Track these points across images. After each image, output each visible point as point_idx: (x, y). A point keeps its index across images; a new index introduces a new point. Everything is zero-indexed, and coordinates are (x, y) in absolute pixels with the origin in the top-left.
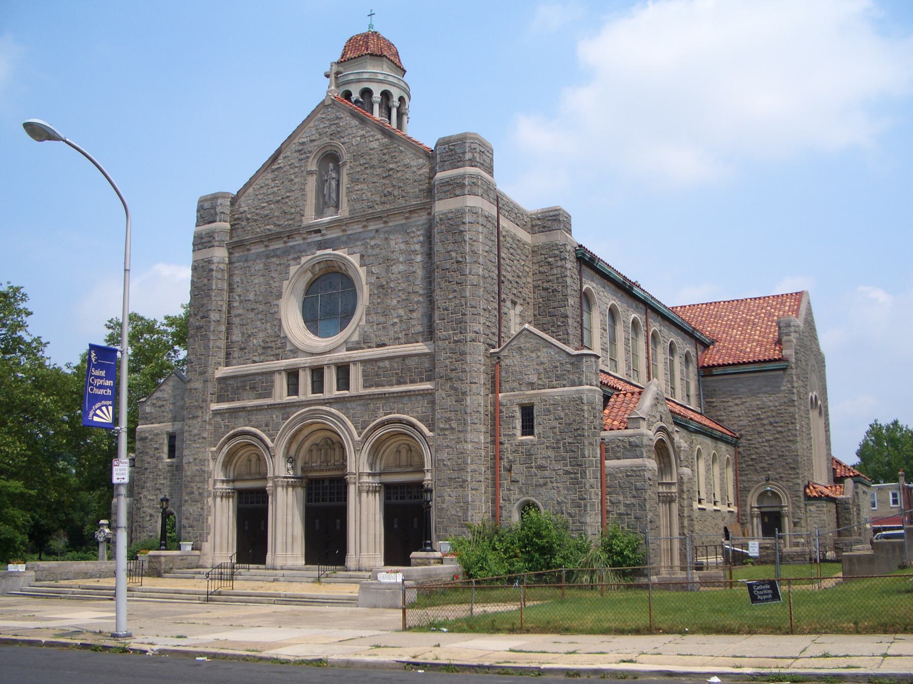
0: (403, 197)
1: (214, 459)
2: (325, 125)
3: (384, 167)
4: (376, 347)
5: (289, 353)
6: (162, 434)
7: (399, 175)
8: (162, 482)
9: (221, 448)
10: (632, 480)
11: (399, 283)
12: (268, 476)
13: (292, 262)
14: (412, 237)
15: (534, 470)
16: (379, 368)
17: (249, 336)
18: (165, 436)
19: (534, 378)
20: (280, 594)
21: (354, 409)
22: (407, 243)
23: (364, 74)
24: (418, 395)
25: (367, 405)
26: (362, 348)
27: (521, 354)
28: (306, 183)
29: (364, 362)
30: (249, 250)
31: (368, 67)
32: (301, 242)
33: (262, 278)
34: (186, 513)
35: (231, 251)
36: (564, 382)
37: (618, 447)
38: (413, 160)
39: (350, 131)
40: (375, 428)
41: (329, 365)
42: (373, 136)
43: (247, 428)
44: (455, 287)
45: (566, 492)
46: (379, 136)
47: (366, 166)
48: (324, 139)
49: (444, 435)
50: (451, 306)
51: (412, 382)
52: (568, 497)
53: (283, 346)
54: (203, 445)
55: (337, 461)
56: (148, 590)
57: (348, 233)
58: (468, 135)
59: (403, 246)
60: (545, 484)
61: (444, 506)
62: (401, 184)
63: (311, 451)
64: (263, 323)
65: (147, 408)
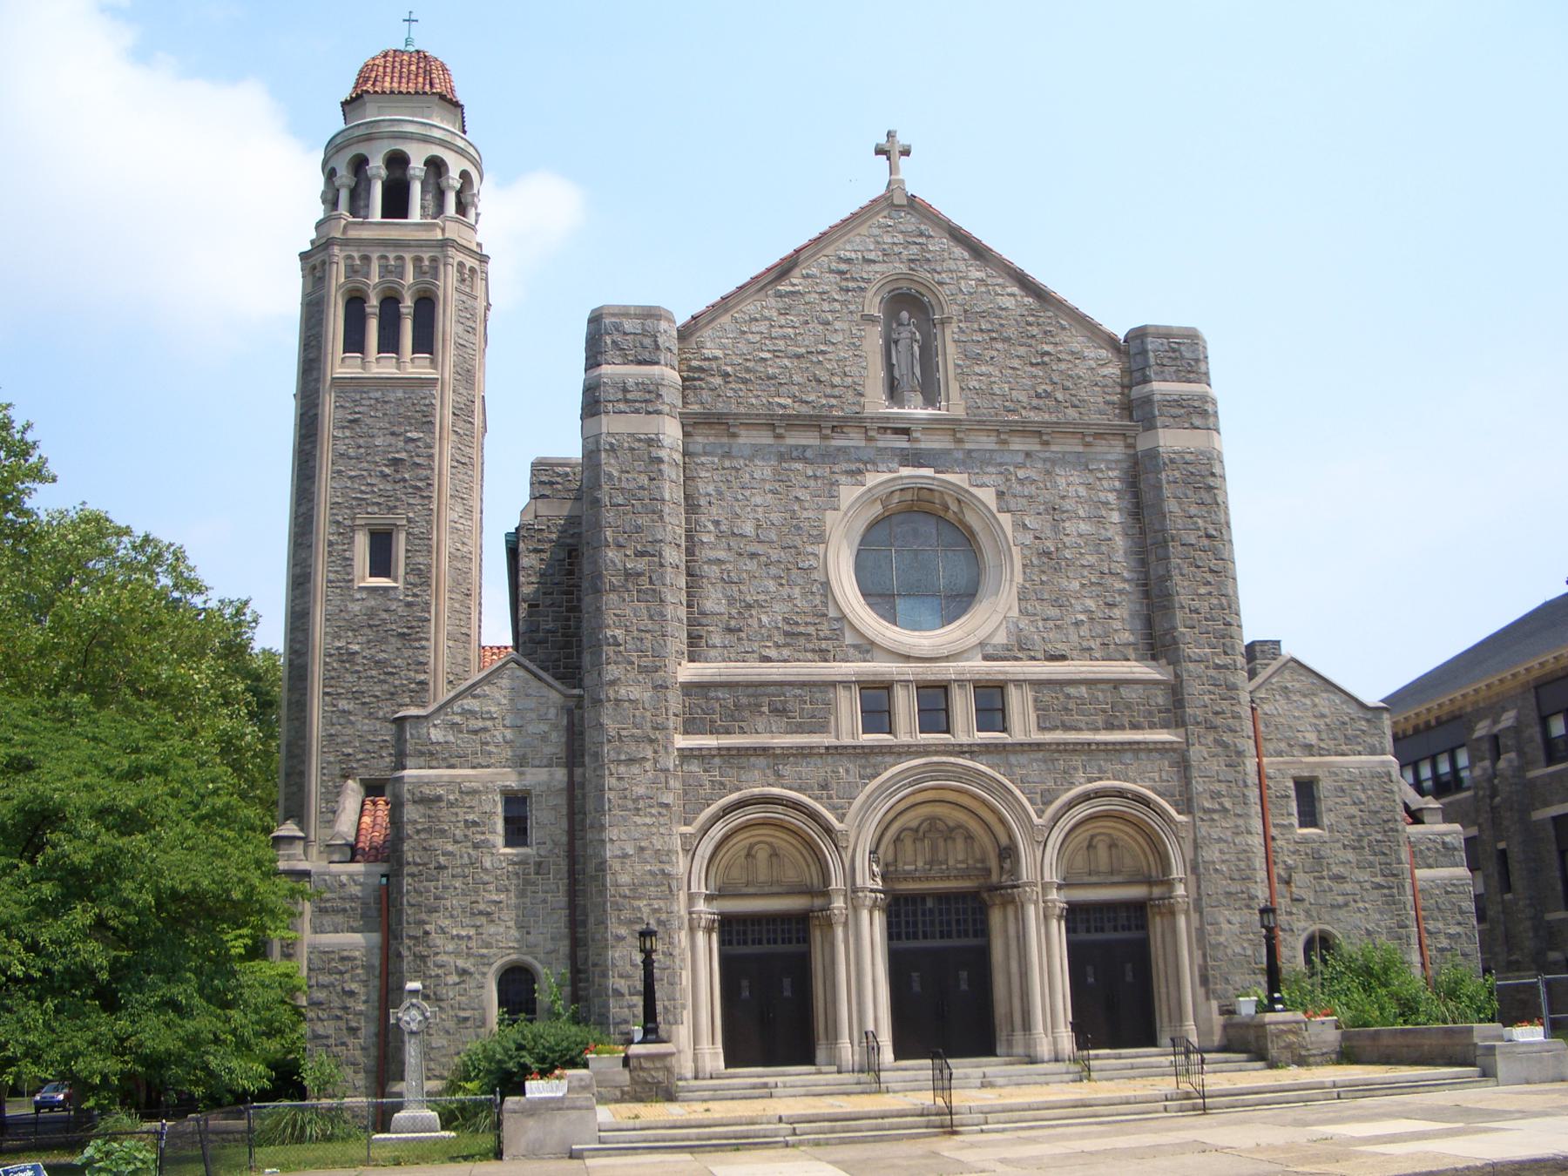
0: (1074, 406)
1: (691, 852)
2: (896, 240)
3: (1030, 346)
4: (1047, 659)
5: (852, 650)
6: (487, 791)
7: (1063, 366)
8: (496, 898)
9: (705, 831)
10: (1454, 898)
11: (1081, 554)
12: (833, 886)
13: (843, 479)
14: (1100, 479)
15: (1326, 882)
16: (1068, 696)
17: (749, 606)
18: (498, 798)
19: (1312, 738)
20: (1323, 1082)
21: (1022, 766)
22: (1088, 486)
23: (435, 130)
24: (1151, 751)
25: (1053, 761)
26: (1016, 659)
27: (1288, 698)
28: (864, 337)
29: (1038, 684)
30: (734, 435)
31: (368, 112)
32: (863, 443)
33: (770, 495)
34: (620, 963)
35: (689, 429)
36: (1360, 748)
37: (1428, 849)
38: (1088, 347)
39: (952, 265)
40: (1070, 805)
41: (961, 683)
42: (1004, 287)
43: (776, 791)
44: (1209, 577)
45: (1378, 916)
46: (1015, 290)
47: (994, 335)
48: (897, 265)
49: (1213, 820)
50: (1204, 607)
51: (1135, 727)
52: (1382, 924)
53: (837, 635)
54: (662, 820)
55: (961, 862)
56: (1000, 1108)
57: (968, 446)
58: (1150, 330)
59: (1082, 491)
60: (1346, 904)
61: (1222, 939)
62: (1069, 384)
63: (897, 840)
64: (782, 585)
65: (432, 730)
